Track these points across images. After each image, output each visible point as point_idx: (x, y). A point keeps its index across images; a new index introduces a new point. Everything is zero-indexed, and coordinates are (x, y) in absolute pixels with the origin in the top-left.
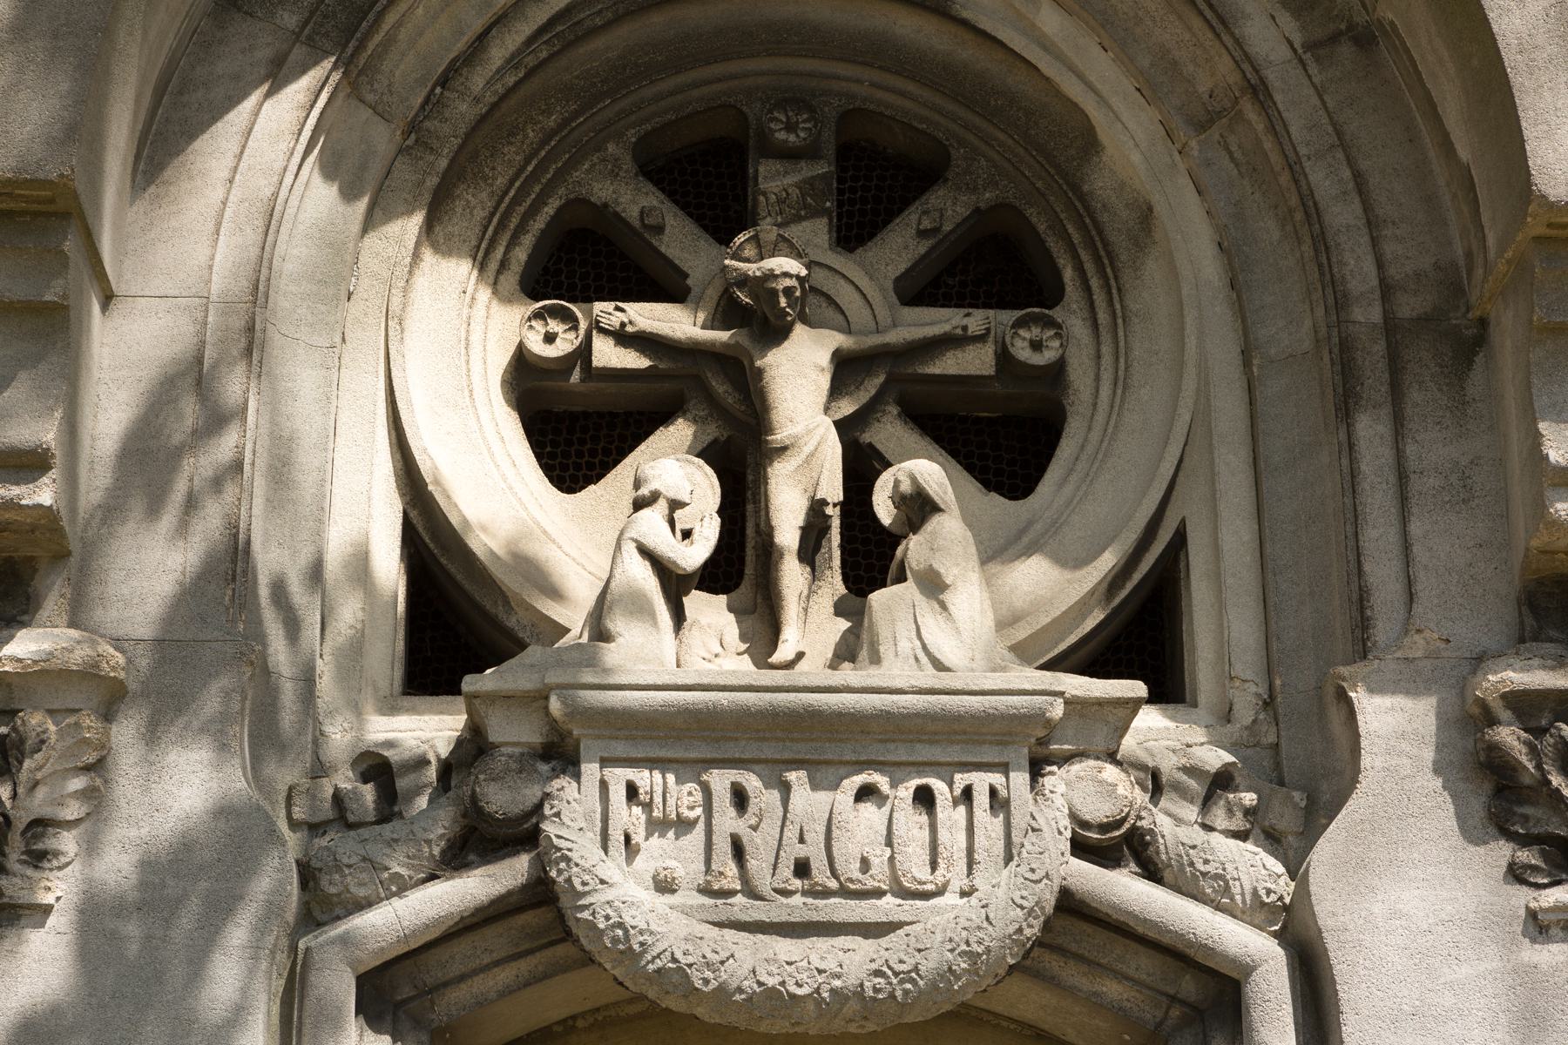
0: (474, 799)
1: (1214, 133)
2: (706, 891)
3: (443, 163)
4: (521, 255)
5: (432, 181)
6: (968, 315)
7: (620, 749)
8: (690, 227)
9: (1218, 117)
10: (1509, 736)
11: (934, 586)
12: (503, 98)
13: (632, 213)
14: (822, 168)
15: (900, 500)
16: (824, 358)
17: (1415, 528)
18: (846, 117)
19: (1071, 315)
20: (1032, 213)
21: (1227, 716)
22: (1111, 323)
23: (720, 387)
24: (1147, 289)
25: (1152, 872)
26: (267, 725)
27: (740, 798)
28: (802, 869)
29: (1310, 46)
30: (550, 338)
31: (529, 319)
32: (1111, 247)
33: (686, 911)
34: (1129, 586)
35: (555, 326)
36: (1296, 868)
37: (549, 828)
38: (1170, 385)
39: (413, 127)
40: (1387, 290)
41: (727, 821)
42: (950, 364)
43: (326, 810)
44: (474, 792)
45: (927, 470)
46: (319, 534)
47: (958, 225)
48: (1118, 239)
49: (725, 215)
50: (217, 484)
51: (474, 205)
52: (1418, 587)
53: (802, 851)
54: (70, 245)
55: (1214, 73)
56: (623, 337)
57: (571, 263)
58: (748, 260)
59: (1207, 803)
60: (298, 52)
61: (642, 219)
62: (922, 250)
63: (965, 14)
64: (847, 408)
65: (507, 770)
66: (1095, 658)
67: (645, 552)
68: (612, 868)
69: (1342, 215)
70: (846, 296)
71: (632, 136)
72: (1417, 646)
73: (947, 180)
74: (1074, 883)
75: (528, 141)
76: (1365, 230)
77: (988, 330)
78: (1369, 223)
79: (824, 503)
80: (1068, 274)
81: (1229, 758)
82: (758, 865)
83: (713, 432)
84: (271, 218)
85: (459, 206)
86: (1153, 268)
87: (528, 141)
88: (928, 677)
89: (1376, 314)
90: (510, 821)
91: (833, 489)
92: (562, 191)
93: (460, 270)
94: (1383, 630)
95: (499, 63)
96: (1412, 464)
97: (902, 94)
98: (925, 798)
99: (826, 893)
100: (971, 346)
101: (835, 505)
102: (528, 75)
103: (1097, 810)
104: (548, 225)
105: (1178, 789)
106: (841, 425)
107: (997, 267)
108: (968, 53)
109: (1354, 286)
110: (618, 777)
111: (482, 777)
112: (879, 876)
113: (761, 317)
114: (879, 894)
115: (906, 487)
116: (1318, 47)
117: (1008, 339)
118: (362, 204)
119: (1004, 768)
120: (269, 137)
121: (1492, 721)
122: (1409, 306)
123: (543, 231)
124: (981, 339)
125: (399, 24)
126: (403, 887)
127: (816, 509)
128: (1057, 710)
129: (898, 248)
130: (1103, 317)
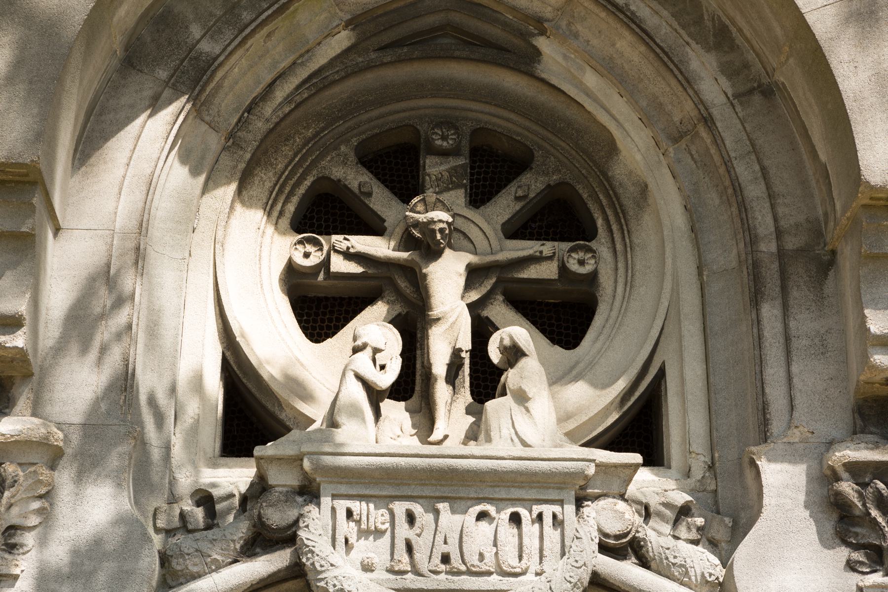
0: (260, 516)
1: (683, 144)
2: (391, 571)
3: (248, 156)
4: (291, 208)
5: (242, 166)
6: (543, 245)
7: (343, 489)
8: (387, 193)
9: (689, 134)
10: (847, 487)
11: (522, 398)
12: (282, 120)
13: (354, 185)
14: (461, 161)
15: (504, 350)
16: (461, 268)
17: (795, 369)
18: (475, 132)
19: (601, 245)
20: (580, 188)
21: (688, 474)
22: (625, 250)
23: (402, 284)
24: (644, 232)
25: (644, 563)
26: (145, 476)
27: (411, 518)
28: (446, 559)
29: (736, 96)
30: (307, 255)
31: (295, 244)
32: (625, 208)
33: (379, 583)
34: (633, 399)
35: (309, 248)
36: (726, 562)
37: (302, 534)
38: (656, 287)
39: (231, 135)
40: (779, 233)
41: (403, 531)
42: (532, 272)
43: (176, 522)
44: (260, 512)
45: (516, 331)
46: (174, 366)
47: (538, 194)
48: (628, 203)
49: (406, 188)
50: (119, 336)
51: (265, 179)
52: (796, 402)
53: (445, 549)
54: (37, 200)
55: (683, 110)
56: (348, 255)
57: (321, 213)
58: (419, 213)
59: (676, 523)
60: (167, 93)
61: (360, 189)
62: (518, 208)
63: (544, 76)
64: (474, 296)
65: (279, 501)
66: (613, 441)
67: (359, 377)
68: (337, 556)
69: (754, 191)
70: (474, 233)
71: (355, 142)
72: (795, 435)
73: (532, 168)
74: (600, 569)
75: (296, 144)
76: (767, 200)
77: (554, 253)
78: (769, 196)
79: (460, 350)
80: (600, 222)
81: (689, 498)
82: (421, 556)
83: (398, 309)
84: (150, 186)
85: (257, 180)
86: (647, 219)
87: (296, 144)
88: (519, 450)
89: (773, 247)
90: (280, 530)
91: (465, 343)
92: (315, 172)
93: (257, 216)
94: (776, 426)
95: (280, 100)
96: (793, 332)
97: (508, 120)
98: (516, 519)
99: (459, 573)
100: (545, 262)
101: (467, 352)
102: (297, 107)
103: (614, 527)
104: (307, 191)
105: (659, 515)
106: (470, 306)
107: (560, 218)
108: (544, 97)
109: (761, 231)
110: (342, 505)
111: (264, 504)
112: (489, 564)
113: (426, 245)
114: (489, 573)
115: (507, 342)
116: (741, 97)
117: (565, 259)
118: (202, 179)
119: (561, 503)
120: (151, 138)
121: (838, 479)
122: (792, 243)
123: (304, 195)
124: (550, 258)
125: (224, 78)
126: (219, 567)
127: (456, 353)
128: (591, 470)
129: (504, 207)
130: (619, 247)
